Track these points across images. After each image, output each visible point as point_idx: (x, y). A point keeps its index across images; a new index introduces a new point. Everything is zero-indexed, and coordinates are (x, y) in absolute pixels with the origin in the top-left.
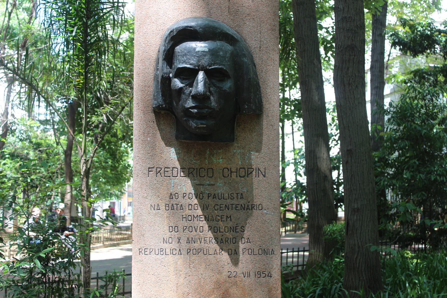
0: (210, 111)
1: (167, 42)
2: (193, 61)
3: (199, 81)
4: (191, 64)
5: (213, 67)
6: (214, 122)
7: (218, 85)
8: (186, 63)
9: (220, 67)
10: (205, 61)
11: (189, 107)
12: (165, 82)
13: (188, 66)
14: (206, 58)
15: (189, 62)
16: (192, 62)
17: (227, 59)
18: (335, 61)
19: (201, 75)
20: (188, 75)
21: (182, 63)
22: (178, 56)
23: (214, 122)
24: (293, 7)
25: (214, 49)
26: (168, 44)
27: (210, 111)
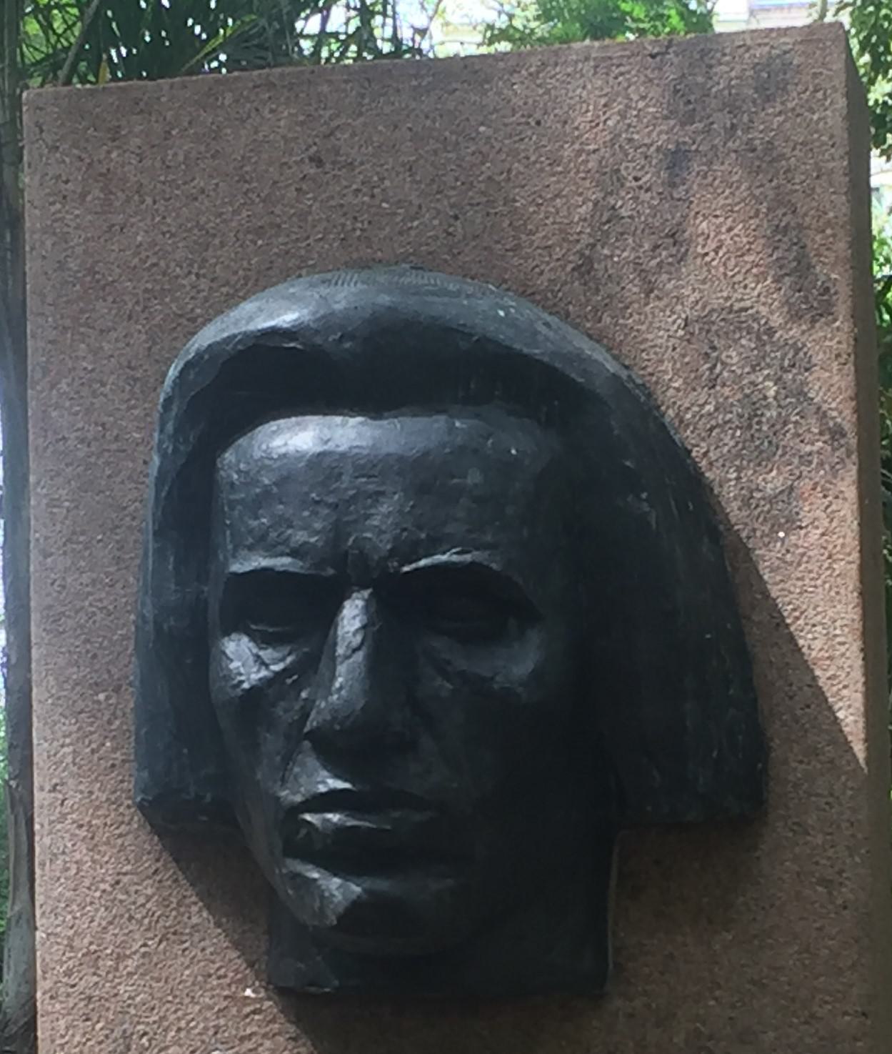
0: (418, 817)
1: (170, 427)
2: (308, 532)
3: (340, 650)
4: (294, 553)
5: (423, 563)
6: (450, 882)
7: (461, 663)
8: (272, 550)
9: (468, 558)
10: (381, 523)
11: (298, 799)
12: (178, 652)
13: (282, 562)
14: (384, 509)
15: (286, 542)
16: (300, 537)
17: (510, 510)
18: (275, 419)
19: (352, 617)
20: (290, 611)
21: (251, 548)
22: (232, 504)
23: (450, 882)
24: (663, 425)
25: (426, 454)
26: (174, 437)
27: (418, 817)
